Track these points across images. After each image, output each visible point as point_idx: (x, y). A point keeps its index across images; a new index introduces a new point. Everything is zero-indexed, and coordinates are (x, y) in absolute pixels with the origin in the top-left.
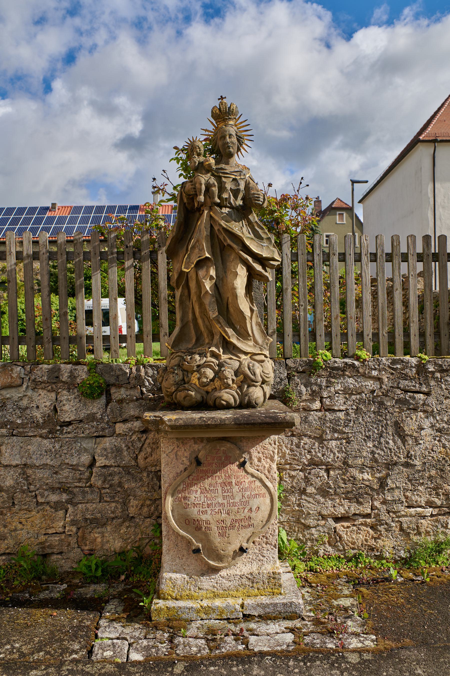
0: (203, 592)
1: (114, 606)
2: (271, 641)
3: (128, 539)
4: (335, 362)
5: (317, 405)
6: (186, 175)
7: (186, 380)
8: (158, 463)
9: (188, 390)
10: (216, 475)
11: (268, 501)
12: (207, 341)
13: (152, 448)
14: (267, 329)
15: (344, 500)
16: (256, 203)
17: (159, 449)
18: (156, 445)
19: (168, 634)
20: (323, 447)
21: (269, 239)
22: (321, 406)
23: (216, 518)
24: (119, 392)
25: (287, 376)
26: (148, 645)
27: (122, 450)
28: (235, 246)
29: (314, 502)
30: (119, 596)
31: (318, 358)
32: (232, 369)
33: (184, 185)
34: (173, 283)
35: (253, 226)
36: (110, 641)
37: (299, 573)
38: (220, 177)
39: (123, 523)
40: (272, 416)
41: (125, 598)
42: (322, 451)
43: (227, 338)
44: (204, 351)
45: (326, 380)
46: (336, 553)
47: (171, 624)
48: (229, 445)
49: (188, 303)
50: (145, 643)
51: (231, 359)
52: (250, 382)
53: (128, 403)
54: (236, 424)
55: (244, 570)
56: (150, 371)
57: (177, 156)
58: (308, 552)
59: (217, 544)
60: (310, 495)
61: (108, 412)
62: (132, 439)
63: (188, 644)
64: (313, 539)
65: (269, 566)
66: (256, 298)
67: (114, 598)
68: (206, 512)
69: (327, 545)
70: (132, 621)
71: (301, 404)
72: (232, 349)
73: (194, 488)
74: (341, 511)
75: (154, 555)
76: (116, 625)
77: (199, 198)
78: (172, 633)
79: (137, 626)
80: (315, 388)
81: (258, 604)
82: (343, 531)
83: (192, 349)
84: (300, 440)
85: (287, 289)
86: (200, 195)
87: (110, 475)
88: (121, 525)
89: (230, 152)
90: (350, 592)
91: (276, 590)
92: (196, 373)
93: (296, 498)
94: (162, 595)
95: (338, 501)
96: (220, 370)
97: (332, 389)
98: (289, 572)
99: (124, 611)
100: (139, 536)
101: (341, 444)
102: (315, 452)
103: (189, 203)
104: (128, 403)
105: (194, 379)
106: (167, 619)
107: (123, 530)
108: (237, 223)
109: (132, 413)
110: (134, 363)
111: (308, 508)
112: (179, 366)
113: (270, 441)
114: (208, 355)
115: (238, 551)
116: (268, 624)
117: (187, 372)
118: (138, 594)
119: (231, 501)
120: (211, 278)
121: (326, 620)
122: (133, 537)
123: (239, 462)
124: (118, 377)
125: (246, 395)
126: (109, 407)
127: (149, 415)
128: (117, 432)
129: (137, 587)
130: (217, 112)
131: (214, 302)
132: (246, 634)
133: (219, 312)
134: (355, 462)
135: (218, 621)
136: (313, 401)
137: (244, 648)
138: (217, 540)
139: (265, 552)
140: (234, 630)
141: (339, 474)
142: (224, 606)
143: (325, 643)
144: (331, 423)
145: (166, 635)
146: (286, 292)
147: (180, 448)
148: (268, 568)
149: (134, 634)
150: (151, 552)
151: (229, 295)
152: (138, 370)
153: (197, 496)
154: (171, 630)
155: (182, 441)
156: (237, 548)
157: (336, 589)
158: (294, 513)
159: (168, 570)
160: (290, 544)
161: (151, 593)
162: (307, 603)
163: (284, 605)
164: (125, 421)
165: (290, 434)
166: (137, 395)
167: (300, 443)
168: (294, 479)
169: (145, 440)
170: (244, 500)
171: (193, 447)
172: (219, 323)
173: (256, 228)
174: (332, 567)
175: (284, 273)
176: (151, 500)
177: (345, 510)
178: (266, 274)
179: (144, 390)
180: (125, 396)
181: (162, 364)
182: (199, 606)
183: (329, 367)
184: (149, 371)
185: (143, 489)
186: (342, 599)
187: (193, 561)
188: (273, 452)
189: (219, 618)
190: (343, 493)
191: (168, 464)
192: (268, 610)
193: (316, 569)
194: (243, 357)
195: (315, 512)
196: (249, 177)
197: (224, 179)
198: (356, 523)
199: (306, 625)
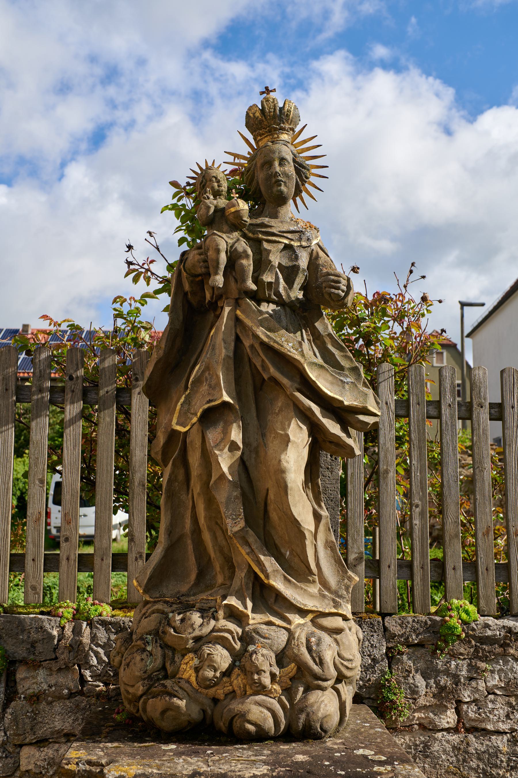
4: (487, 626)
5: (449, 718)
6: (193, 240)
7: (170, 669)
9: (172, 695)
12: (220, 579)
14: (346, 555)
16: (330, 294)
21: (355, 370)
22: (459, 721)
24: (33, 677)
28: (285, 381)
32: (271, 648)
33: (185, 257)
34: (156, 453)
35: (324, 343)
38: (259, 242)
43: (262, 576)
44: (212, 604)
45: (469, 665)
49: (184, 497)
51: (269, 623)
52: (310, 679)
53: (50, 703)
56: (102, 635)
57: (175, 201)
66: (325, 488)
71: (416, 715)
72: (272, 600)
77: (214, 280)
80: (444, 680)
83: (188, 595)
85: (387, 472)
86: (216, 273)
89: (281, 192)
92: (191, 655)
96: (246, 651)
97: (481, 685)
103: (193, 293)
104: (51, 703)
105: (187, 668)
108: (292, 335)
109: (58, 725)
110: (70, 616)
112: (157, 634)
114: (221, 613)
117: (172, 651)
120: (233, 446)
125: (302, 711)
126: (9, 711)
128: (23, 768)
130: (258, 114)
131: (236, 497)
133: (246, 521)
136: (440, 708)
144: (479, 759)
146: (385, 478)
151: (270, 484)
152: (77, 631)
164: (41, 743)
166: (71, 685)
172: (247, 543)
173: (330, 347)
175: (381, 440)
178: (350, 442)
179: (87, 673)
180: (45, 687)
181: (127, 620)
183: (474, 637)
184: (99, 635)
194: (297, 620)
196: (318, 244)
197: (266, 245)
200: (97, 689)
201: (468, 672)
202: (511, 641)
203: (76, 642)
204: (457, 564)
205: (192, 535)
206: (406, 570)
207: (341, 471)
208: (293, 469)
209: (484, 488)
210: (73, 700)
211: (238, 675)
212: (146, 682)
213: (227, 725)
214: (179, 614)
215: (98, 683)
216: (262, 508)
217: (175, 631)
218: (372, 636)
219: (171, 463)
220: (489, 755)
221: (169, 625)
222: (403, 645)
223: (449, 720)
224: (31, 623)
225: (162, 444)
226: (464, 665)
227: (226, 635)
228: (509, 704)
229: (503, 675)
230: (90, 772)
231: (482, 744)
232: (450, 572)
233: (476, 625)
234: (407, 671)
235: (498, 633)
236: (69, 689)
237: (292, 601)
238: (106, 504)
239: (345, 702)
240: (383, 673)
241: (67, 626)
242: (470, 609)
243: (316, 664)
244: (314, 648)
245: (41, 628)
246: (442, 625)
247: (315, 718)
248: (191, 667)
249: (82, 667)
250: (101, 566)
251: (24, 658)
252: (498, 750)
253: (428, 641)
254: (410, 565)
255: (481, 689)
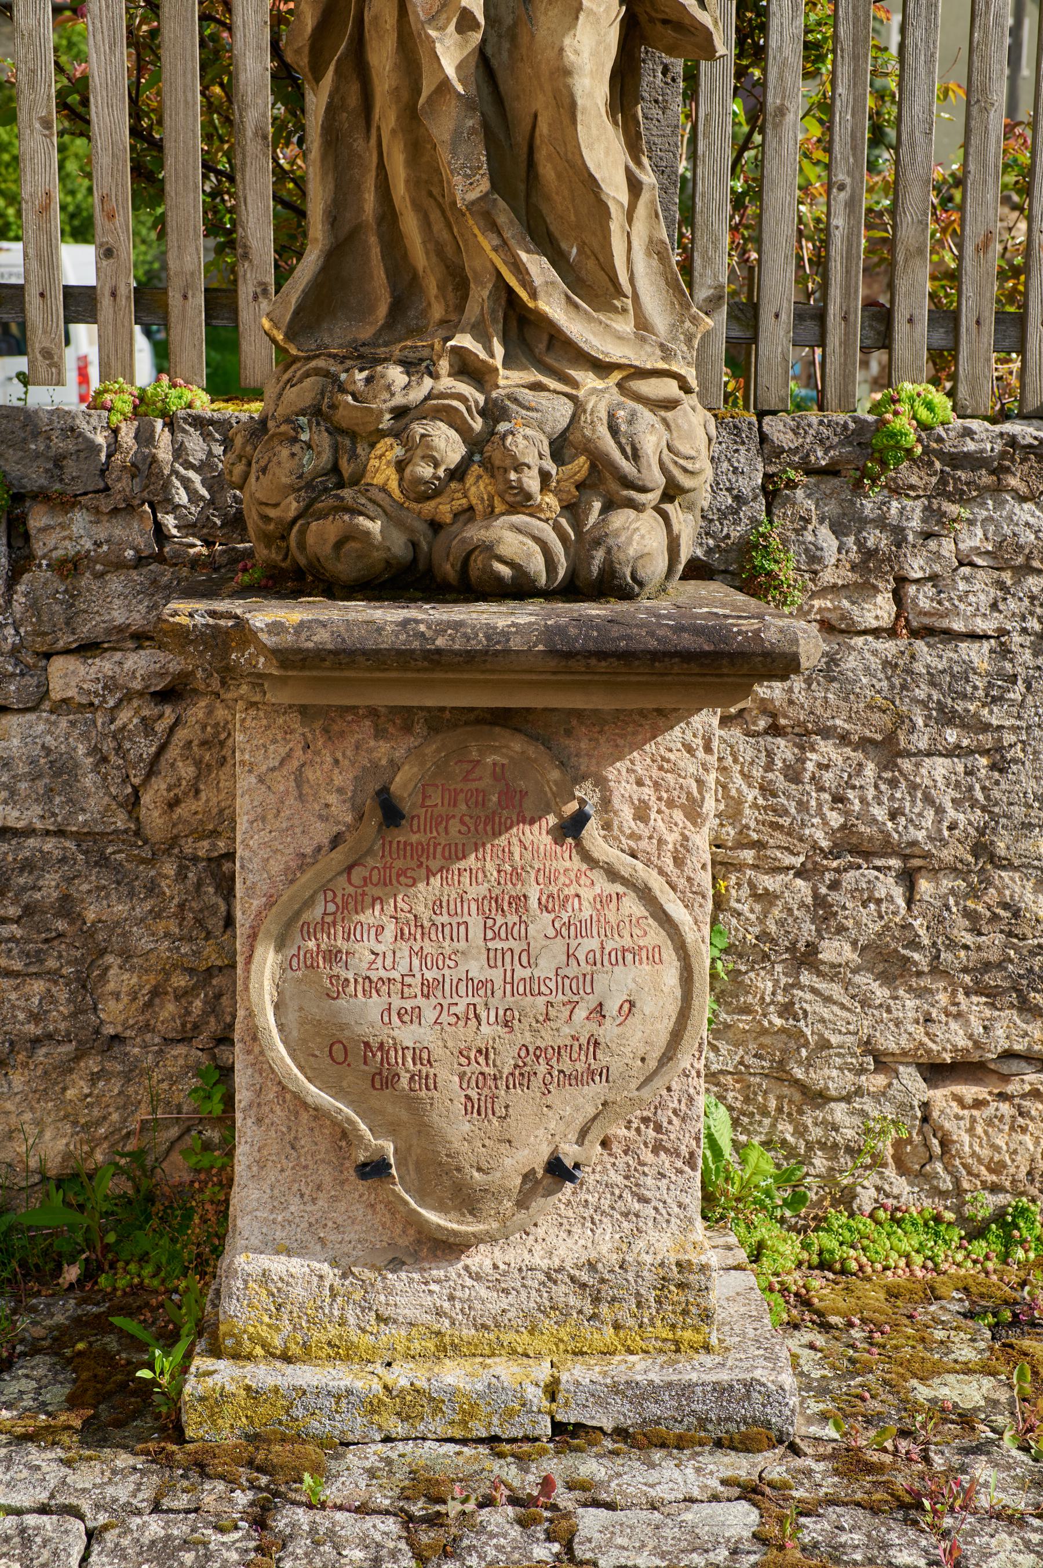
0: (397, 1334)
1: (34, 1384)
2: (667, 1532)
3: (98, 1123)
4: (968, 433)
5: (880, 609)
7: (347, 468)
8: (222, 823)
10: (462, 864)
11: (670, 976)
12: (437, 312)
13: (198, 763)
15: (967, 994)
17: (227, 769)
18: (215, 751)
19: (250, 1495)
20: (893, 783)
22: (898, 616)
23: (455, 1038)
24: (63, 527)
25: (763, 487)
26: (169, 1537)
27: (77, 766)
29: (846, 1000)
30: (55, 1345)
31: (896, 413)
34: (298, 52)
36: (12, 1520)
37: (776, 1274)
39: (77, 1059)
40: (704, 627)
41: (80, 1354)
42: (892, 798)
43: (523, 295)
44: (426, 353)
45: (926, 509)
46: (927, 1203)
47: (260, 1456)
48: (517, 745)
49: (359, 144)
50: (155, 1527)
51: (537, 387)
52: (613, 486)
54: (552, 653)
55: (562, 1252)
56: (196, 445)
58: (812, 1195)
59: (456, 1145)
60: (834, 972)
61: (17, 608)
62: (119, 723)
63: (331, 1534)
64: (835, 1145)
65: (666, 1238)
67: (35, 1350)
68: (417, 1014)
69: (891, 1172)
70: (102, 1442)
71: (817, 603)
73: (368, 917)
74: (952, 1039)
75: (201, 1190)
76: (35, 1455)
78: (267, 1489)
79: (124, 1460)
80: (875, 538)
81: (615, 1384)
82: (958, 1117)
83: (375, 345)
84: (802, 748)
87: (27, 866)
88: (66, 1068)
90: (981, 1352)
91: (688, 1335)
92: (389, 441)
93: (777, 981)
94: (229, 1342)
95: (943, 998)
96: (493, 433)
97: (947, 547)
98: (738, 1268)
99: (73, 1402)
100: (143, 1113)
101: (969, 773)
102: (863, 800)
105: (382, 467)
106: (248, 1437)
107: (77, 1088)
109: (119, 616)
110: (128, 409)
111: (823, 1021)
112: (319, 413)
113: (689, 736)
114: (444, 365)
115: (540, 1173)
116: (652, 1466)
117: (351, 437)
118: (132, 1337)
119: (521, 973)
121: (888, 1459)
122: (115, 1117)
123: (559, 815)
124: (58, 461)
125: (597, 543)
126: (21, 588)
127: (187, 612)
128: (56, 695)
129: (130, 1312)
131: (473, 131)
132: (564, 1499)
133: (494, 187)
134: (1023, 845)
135: (451, 1448)
136: (865, 590)
137: (557, 1555)
138: (457, 1129)
139: (650, 1181)
140: (516, 1484)
141: (952, 891)
142: (479, 1387)
143: (885, 1546)
144: (933, 684)
145: (242, 1498)
146: (777, 126)
147: (317, 753)
148: (660, 1245)
149: (110, 1491)
150: (187, 1177)
151: (541, 103)
152: (145, 437)
153: (379, 948)
154: (264, 1480)
155: (322, 720)
156: (539, 1162)
157: (923, 1340)
158: (766, 1040)
159: (255, 1241)
160: (743, 1162)
161: (184, 1331)
162: (809, 1388)
163: (721, 1390)
164: (88, 649)
165: (762, 724)
166: (140, 541)
167: (802, 761)
168: (772, 904)
169: (172, 729)
170: (572, 971)
171: (370, 751)
172: (494, 227)
174: (908, 1256)
176: (191, 971)
177: (970, 1037)
179: (170, 521)
180: (89, 545)
182: (377, 1386)
183: (940, 455)
184: (189, 445)
185: (160, 927)
186: (951, 1378)
187: (359, 1211)
188: (700, 782)
189: (458, 1434)
190: (965, 970)
191: (264, 819)
192: (653, 1409)
193: (843, 1261)
194: (588, 380)
195: (850, 1039)
198: (1010, 1089)
199: (808, 1473)
200: (192, 551)
201: (923, 521)
202: (1013, 461)
203: (145, 457)
204: (916, 312)
205: (379, 225)
206: (811, 326)
207: (684, 163)
208: (588, 67)
209: (986, 148)
210: (144, 571)
211: (479, 477)
212: (303, 493)
213: (458, 567)
214: (361, 370)
215: (191, 540)
216: (524, 156)
217: (355, 399)
218: (737, 451)
219: (332, 68)
220: (953, 676)
221: (342, 390)
222: (796, 469)
223: (879, 612)
224: (51, 422)
225: (309, 29)
226: (916, 509)
227: (455, 403)
228: (1001, 585)
229: (992, 528)
230: (216, 627)
231: (941, 657)
232: (901, 328)
233: (947, 430)
234: (802, 518)
235: (989, 447)
236: (137, 551)
237: (582, 345)
238: (186, 177)
239: (678, 537)
240: (755, 522)
241: (123, 425)
242: (936, 401)
243: (627, 458)
244: (623, 427)
245: (72, 430)
246: (877, 430)
247: (622, 556)
248: (389, 462)
249: (159, 508)
250: (184, 310)
251: (41, 487)
252: (970, 668)
253: (849, 462)
254: (820, 317)
255: (947, 554)
